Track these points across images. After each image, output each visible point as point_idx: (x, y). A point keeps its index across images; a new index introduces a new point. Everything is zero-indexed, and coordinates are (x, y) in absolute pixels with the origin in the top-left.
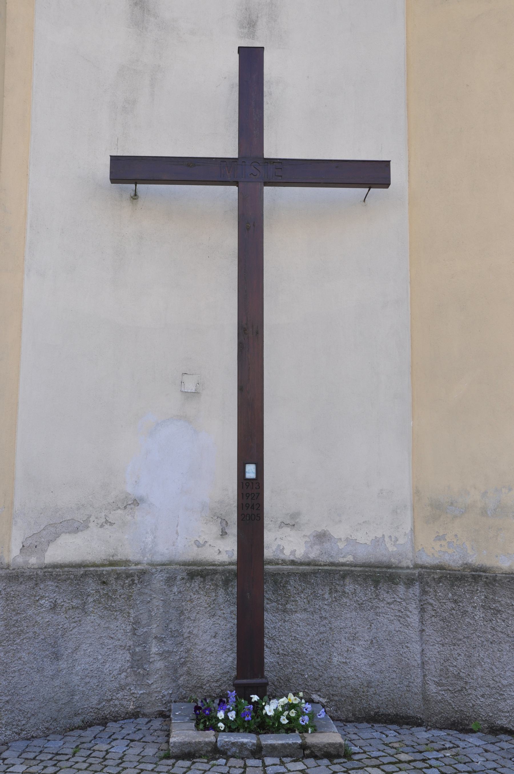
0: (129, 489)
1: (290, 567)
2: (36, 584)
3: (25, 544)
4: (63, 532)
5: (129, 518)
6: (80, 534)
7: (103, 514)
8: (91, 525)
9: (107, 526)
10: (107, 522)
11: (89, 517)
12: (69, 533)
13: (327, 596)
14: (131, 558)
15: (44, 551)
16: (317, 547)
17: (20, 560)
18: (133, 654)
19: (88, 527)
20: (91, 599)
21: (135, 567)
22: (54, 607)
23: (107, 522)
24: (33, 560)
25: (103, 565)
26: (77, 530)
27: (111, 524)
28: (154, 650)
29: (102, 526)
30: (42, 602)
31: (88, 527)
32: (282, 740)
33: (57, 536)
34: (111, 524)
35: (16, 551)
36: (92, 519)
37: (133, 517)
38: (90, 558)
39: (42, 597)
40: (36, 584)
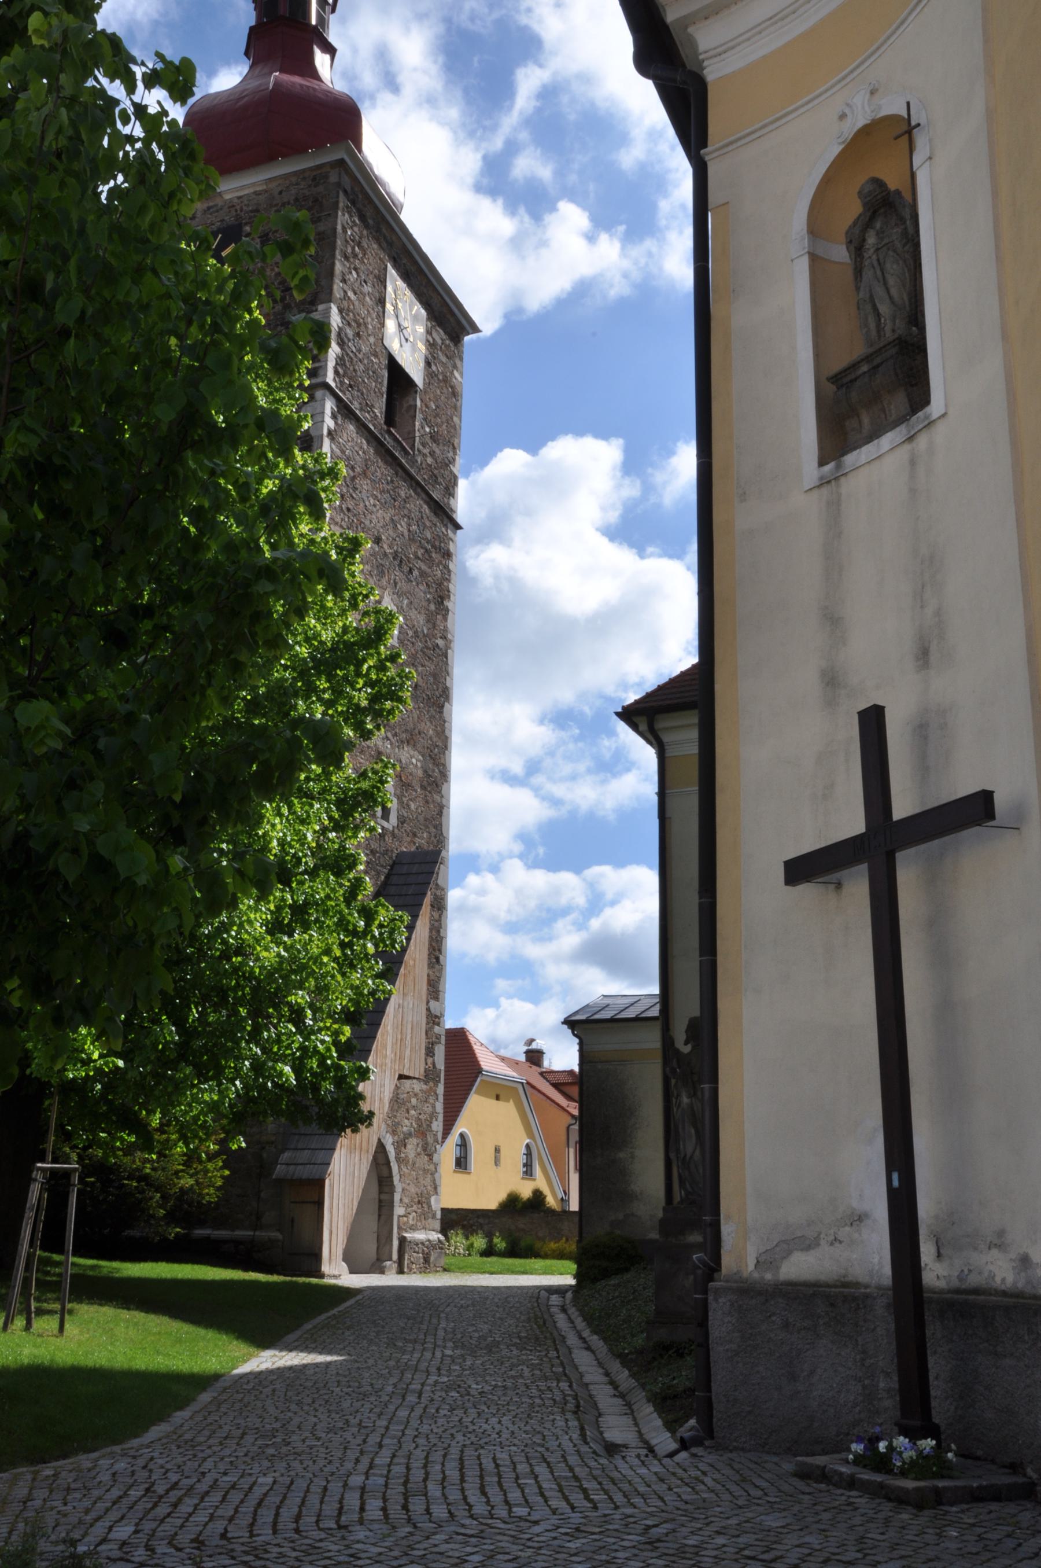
0: (855, 1204)
1: (1000, 1299)
2: (767, 1300)
3: (761, 1259)
4: (797, 1249)
5: (856, 1235)
6: (812, 1252)
7: (832, 1231)
8: (822, 1242)
9: (837, 1244)
10: (836, 1239)
11: (820, 1234)
12: (802, 1250)
13: (1026, 1338)
14: (860, 1280)
15: (778, 1268)
16: (1023, 1274)
17: (756, 1275)
18: (864, 1387)
19: (819, 1245)
20: (821, 1322)
21: (863, 1290)
22: (786, 1325)
23: (836, 1239)
24: (768, 1276)
25: (835, 1286)
26: (808, 1248)
27: (841, 1242)
28: (882, 1385)
29: (832, 1244)
30: (774, 1318)
31: (819, 1245)
32: (309, 1284)
33: (789, 1253)
34: (841, 1242)
35: (751, 1266)
36: (822, 1236)
37: (860, 1234)
38: (823, 1278)
39: (774, 1314)
40: (767, 1300)
